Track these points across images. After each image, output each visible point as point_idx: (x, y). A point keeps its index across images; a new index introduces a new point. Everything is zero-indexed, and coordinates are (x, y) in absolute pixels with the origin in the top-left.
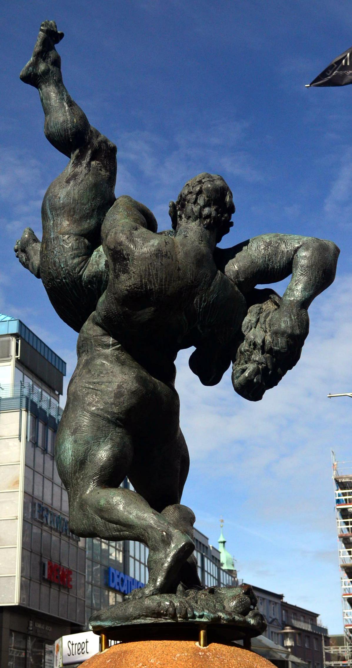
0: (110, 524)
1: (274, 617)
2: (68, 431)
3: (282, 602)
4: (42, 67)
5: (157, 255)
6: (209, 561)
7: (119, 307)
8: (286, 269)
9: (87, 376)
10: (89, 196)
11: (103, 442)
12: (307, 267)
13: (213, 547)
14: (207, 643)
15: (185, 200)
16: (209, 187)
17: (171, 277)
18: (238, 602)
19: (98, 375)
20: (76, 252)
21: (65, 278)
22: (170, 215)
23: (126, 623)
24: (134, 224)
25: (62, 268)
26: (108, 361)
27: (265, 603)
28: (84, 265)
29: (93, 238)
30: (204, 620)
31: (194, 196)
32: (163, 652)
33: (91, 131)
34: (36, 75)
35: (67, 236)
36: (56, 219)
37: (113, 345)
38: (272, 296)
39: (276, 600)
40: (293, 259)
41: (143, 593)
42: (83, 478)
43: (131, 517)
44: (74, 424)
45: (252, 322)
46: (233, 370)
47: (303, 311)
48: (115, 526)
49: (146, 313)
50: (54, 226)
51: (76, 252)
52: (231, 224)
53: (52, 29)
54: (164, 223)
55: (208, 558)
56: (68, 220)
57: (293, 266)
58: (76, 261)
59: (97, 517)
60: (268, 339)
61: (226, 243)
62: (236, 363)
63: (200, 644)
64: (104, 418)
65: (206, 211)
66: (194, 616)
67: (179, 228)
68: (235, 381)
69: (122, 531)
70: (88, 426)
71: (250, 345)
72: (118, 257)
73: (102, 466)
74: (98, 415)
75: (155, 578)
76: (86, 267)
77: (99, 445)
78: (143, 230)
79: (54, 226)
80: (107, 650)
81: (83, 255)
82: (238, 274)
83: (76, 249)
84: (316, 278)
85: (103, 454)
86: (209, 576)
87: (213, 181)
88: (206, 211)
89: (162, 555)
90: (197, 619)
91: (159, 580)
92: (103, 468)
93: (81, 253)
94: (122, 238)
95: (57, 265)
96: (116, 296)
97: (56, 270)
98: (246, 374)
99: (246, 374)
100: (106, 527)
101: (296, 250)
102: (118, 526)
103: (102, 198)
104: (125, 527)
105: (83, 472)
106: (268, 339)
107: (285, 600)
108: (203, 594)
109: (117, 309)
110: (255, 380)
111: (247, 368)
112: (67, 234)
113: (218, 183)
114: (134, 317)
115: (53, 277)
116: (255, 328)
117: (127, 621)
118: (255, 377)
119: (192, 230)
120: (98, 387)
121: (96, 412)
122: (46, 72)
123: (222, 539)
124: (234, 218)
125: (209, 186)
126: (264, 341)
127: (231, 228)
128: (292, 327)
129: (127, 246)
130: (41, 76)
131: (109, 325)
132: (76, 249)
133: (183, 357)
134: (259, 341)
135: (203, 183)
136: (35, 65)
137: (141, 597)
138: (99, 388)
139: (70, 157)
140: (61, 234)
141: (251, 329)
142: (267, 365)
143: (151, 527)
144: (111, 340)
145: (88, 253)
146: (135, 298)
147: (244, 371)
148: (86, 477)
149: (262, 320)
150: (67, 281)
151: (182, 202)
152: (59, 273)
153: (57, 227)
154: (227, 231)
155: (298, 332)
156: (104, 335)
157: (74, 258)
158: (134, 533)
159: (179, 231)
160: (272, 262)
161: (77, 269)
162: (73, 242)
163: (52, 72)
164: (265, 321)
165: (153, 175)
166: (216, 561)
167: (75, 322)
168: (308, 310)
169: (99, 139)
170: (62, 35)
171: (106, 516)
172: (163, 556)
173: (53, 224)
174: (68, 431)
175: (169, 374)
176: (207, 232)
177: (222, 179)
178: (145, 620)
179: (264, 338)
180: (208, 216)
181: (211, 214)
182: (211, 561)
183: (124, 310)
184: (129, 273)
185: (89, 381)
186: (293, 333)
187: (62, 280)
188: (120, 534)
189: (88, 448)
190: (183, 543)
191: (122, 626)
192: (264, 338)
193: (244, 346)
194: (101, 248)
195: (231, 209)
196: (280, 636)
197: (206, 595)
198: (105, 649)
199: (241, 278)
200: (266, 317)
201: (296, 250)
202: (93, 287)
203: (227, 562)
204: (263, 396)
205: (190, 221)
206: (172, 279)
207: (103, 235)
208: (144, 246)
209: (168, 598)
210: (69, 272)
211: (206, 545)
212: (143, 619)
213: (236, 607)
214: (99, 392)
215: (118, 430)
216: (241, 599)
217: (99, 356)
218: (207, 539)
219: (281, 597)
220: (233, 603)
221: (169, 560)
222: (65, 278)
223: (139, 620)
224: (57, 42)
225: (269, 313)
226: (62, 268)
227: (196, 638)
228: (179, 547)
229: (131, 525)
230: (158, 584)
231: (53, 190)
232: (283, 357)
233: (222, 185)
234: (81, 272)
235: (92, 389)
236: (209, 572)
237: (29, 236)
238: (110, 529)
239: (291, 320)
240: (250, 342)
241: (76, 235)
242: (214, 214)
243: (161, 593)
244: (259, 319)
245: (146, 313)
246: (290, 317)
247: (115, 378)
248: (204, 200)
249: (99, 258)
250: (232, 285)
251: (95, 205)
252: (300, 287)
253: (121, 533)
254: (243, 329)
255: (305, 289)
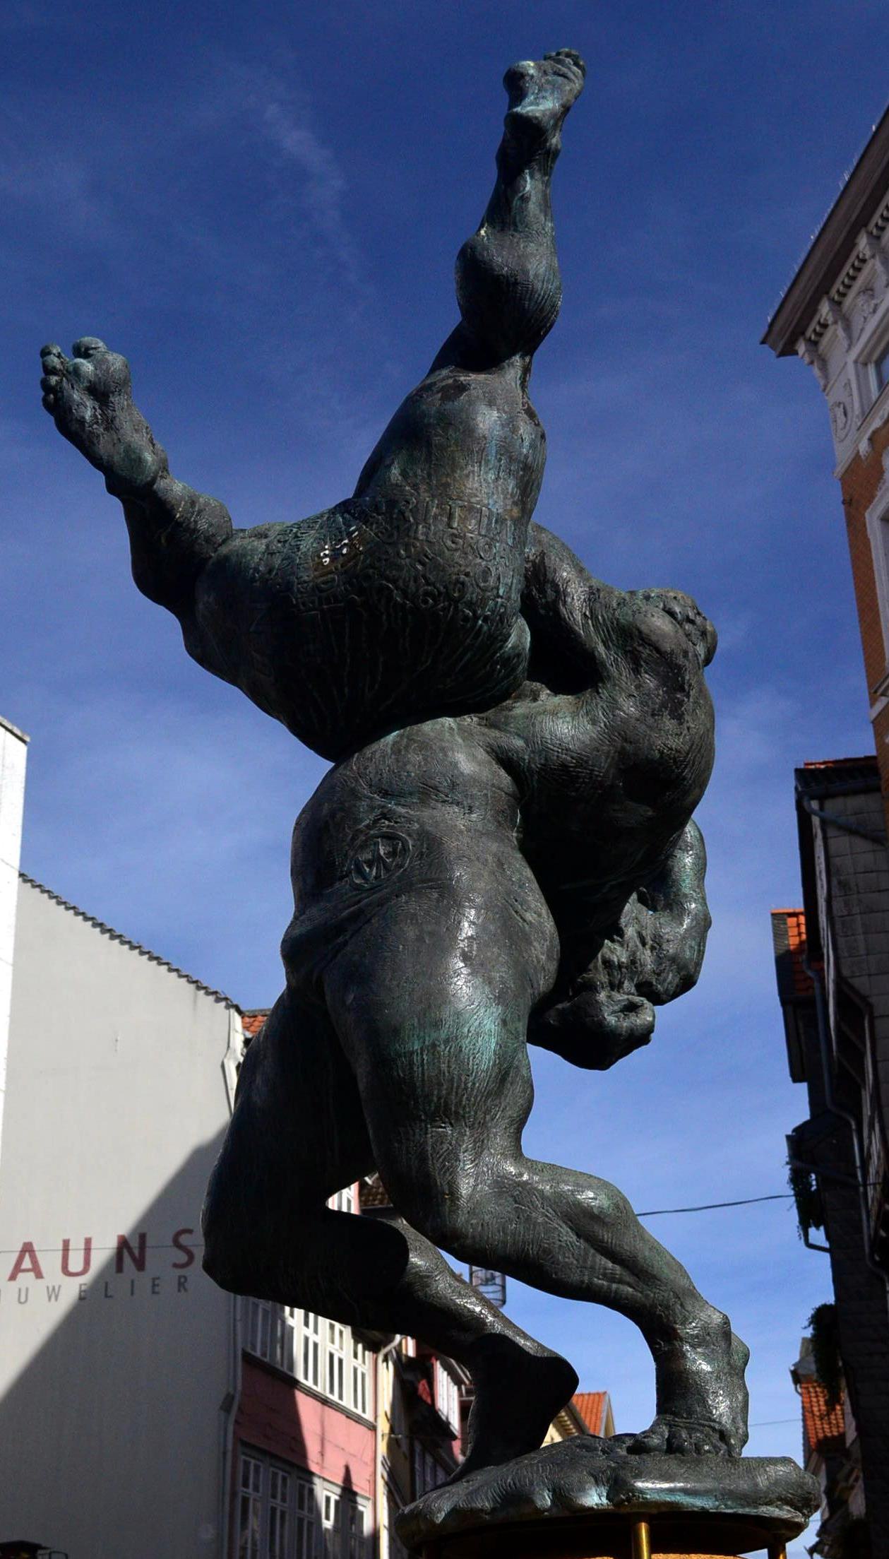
0: (599, 1257)
21: (486, 619)
23: (747, 1510)
25: (498, 596)
48: (610, 1265)
59: (565, 1230)
69: (621, 1282)
96: (627, 746)
100: (585, 1261)
102: (617, 1267)
109: (607, 771)
114: (616, 807)
117: (749, 1505)
150: (485, 628)
152: (483, 602)
158: (647, 1296)
178: (781, 1509)
184: (681, 724)
187: (476, 618)
188: (609, 1288)
191: (735, 1515)
222: (486, 619)
223: (771, 1509)
226: (498, 596)
229: (654, 1277)
238: (592, 1268)
253: (614, 1286)
254: (623, 921)
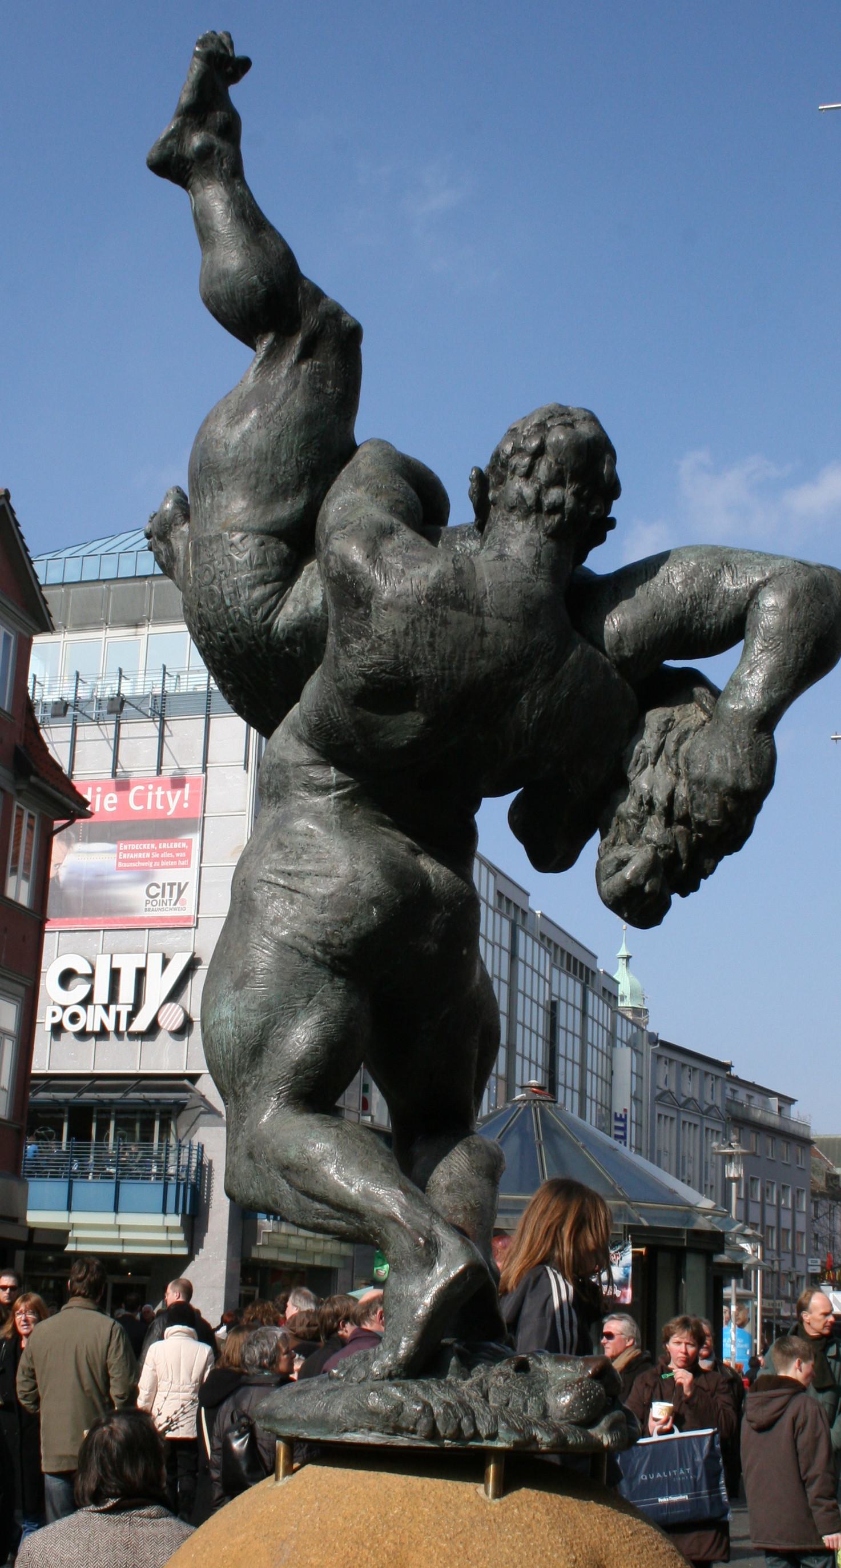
1: (711, 1102)
2: (228, 978)
3: (730, 1076)
4: (196, 141)
5: (430, 599)
6: (596, 998)
7: (346, 710)
8: (733, 630)
9: (275, 856)
10: (293, 442)
11: (303, 1007)
12: (779, 632)
13: (604, 972)
14: (503, 1489)
15: (505, 465)
16: (562, 441)
17: (464, 652)
18: (576, 1399)
19: (299, 858)
20: (258, 572)
22: (471, 498)
24: (386, 518)
26: (321, 825)
27: (697, 1076)
28: (277, 602)
29: (296, 543)
30: (499, 1445)
31: (527, 460)
32: (403, 1510)
33: (303, 289)
34: (182, 159)
35: (238, 536)
36: (218, 495)
37: (339, 786)
38: (698, 691)
39: (716, 1072)
40: (747, 608)
41: (368, 1371)
42: (256, 1085)
43: (353, 1191)
44: (240, 963)
45: (648, 750)
46: (601, 858)
47: (763, 736)
49: (407, 726)
50: (212, 508)
51: (258, 572)
52: (611, 524)
53: (222, 51)
54: (461, 512)
55: (594, 993)
56: (244, 498)
57: (748, 626)
58: (259, 592)
60: (682, 792)
61: (601, 561)
62: (606, 840)
63: (487, 1493)
64: (304, 957)
65: (554, 495)
66: (476, 1436)
67: (490, 529)
68: (604, 884)
70: (269, 972)
71: (641, 804)
72: (349, 592)
73: (298, 1064)
74: (292, 948)
75: (395, 1338)
76: (282, 606)
77: (295, 1014)
78: (406, 535)
79: (212, 508)
80: (287, 1478)
81: (275, 581)
82: (620, 640)
83: (260, 566)
84: (797, 658)
85: (301, 1037)
86: (595, 1024)
87: (572, 425)
88: (554, 495)
89: (414, 1288)
90: (486, 1443)
91: (403, 1344)
92: (299, 1068)
93: (270, 575)
94: (356, 555)
95: (216, 599)
97: (215, 610)
98: (627, 873)
99: (627, 873)
101: (754, 592)
103: (323, 444)
104: (338, 1211)
105: (258, 1072)
106: (682, 792)
107: (734, 1072)
108: (501, 1374)
110: (647, 888)
111: (629, 859)
112: (241, 530)
113: (584, 429)
114: (381, 734)
115: (209, 624)
116: (654, 764)
118: (646, 880)
119: (519, 541)
120: (295, 883)
121: (290, 941)
122: (205, 153)
123: (623, 952)
124: (617, 509)
125: (562, 437)
126: (671, 797)
127: (610, 534)
128: (738, 772)
129: (366, 577)
130: (193, 161)
131: (330, 744)
132: (260, 566)
133: (493, 817)
134: (660, 797)
135: (549, 430)
136: (178, 135)
137: (364, 1379)
138: (301, 887)
139: (255, 350)
140: (225, 529)
141: (645, 766)
142: (676, 850)
143: (394, 1220)
144: (333, 774)
145: (287, 574)
146: (383, 691)
147: (622, 864)
148: (263, 1085)
149: (670, 747)
151: (500, 465)
153: (219, 513)
154: (601, 539)
155: (748, 784)
156: (314, 763)
157: (252, 587)
159: (489, 537)
160: (701, 614)
161: (260, 612)
162: (254, 549)
163: (219, 153)
164: (677, 751)
165: (436, 404)
166: (610, 996)
167: (261, 711)
168: (776, 733)
169: (321, 309)
170: (244, 65)
171: (299, 1182)
172: (417, 1291)
173: (211, 505)
174: (228, 978)
175: (458, 846)
176: (551, 545)
177: (593, 419)
179: (673, 791)
180: (556, 508)
181: (563, 503)
182: (599, 997)
183: (358, 716)
185: (279, 868)
186: (738, 788)
187: (227, 633)
189: (269, 1019)
190: (461, 1267)
192: (673, 791)
193: (628, 806)
194: (314, 564)
195: (612, 490)
196: (720, 1157)
197: (507, 1377)
198: (284, 1475)
199: (626, 649)
200: (679, 742)
201: (754, 592)
202: (295, 651)
203: (631, 994)
204: (665, 918)
205: (513, 517)
206: (467, 655)
207: (320, 538)
208: (403, 576)
209: (420, 1393)
210: (241, 616)
211: (592, 968)
212: (363, 1433)
213: (571, 1408)
214: (298, 896)
215: (340, 982)
216: (584, 1391)
217: (303, 811)
218: (596, 957)
219: (727, 1067)
220: (566, 1399)
221: (428, 1300)
222: (234, 630)
224: (235, 78)
225: (687, 732)
227: (479, 1476)
228: (452, 1274)
230: (402, 1352)
231: (213, 428)
232: (716, 828)
233: (592, 434)
234: (270, 618)
235: (284, 887)
236: (596, 1018)
237: (174, 508)
239: (735, 755)
240: (641, 797)
241: (261, 532)
242: (569, 503)
243: (407, 1378)
244: (663, 743)
245: (407, 726)
246: (733, 748)
247: (338, 862)
248: (550, 468)
249: (308, 593)
250: (605, 665)
251: (306, 466)
252: (758, 678)
255: (768, 685)
